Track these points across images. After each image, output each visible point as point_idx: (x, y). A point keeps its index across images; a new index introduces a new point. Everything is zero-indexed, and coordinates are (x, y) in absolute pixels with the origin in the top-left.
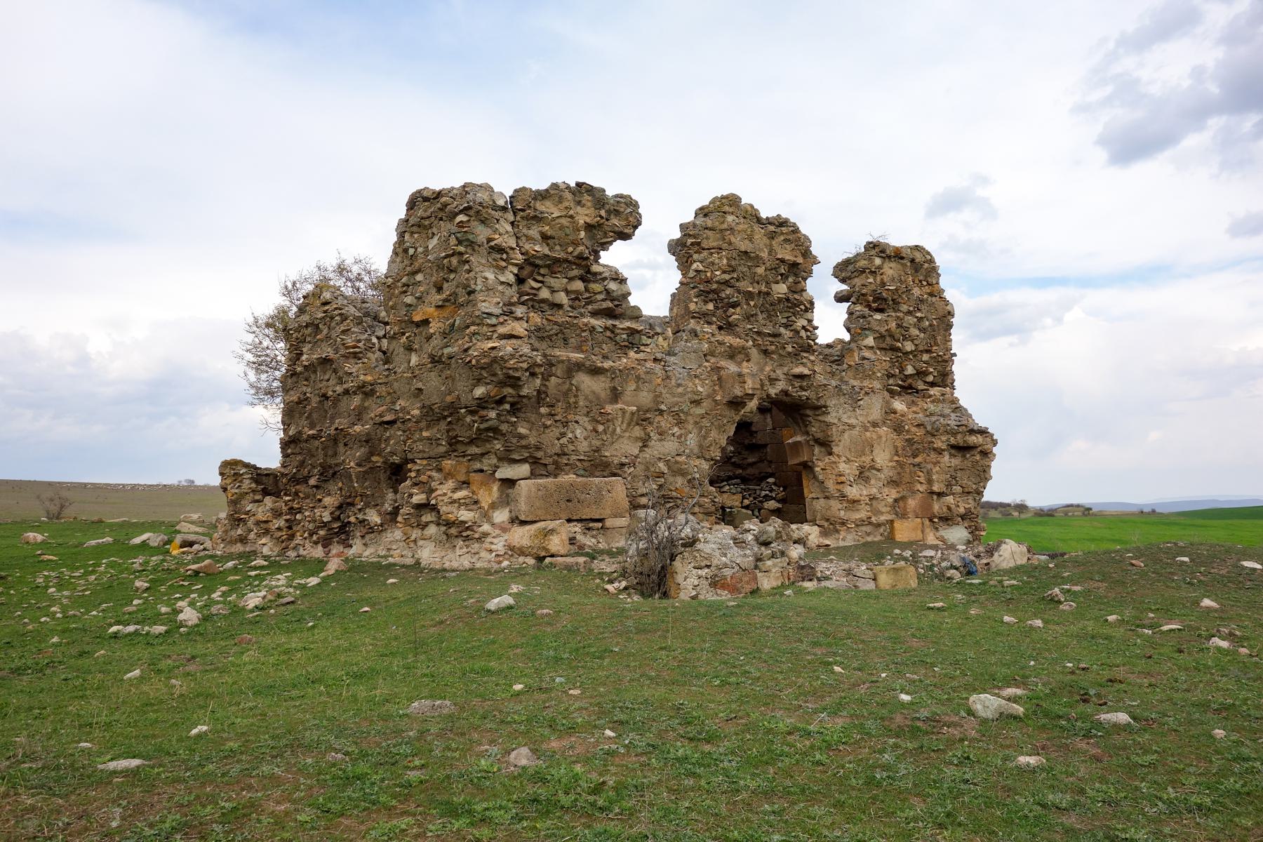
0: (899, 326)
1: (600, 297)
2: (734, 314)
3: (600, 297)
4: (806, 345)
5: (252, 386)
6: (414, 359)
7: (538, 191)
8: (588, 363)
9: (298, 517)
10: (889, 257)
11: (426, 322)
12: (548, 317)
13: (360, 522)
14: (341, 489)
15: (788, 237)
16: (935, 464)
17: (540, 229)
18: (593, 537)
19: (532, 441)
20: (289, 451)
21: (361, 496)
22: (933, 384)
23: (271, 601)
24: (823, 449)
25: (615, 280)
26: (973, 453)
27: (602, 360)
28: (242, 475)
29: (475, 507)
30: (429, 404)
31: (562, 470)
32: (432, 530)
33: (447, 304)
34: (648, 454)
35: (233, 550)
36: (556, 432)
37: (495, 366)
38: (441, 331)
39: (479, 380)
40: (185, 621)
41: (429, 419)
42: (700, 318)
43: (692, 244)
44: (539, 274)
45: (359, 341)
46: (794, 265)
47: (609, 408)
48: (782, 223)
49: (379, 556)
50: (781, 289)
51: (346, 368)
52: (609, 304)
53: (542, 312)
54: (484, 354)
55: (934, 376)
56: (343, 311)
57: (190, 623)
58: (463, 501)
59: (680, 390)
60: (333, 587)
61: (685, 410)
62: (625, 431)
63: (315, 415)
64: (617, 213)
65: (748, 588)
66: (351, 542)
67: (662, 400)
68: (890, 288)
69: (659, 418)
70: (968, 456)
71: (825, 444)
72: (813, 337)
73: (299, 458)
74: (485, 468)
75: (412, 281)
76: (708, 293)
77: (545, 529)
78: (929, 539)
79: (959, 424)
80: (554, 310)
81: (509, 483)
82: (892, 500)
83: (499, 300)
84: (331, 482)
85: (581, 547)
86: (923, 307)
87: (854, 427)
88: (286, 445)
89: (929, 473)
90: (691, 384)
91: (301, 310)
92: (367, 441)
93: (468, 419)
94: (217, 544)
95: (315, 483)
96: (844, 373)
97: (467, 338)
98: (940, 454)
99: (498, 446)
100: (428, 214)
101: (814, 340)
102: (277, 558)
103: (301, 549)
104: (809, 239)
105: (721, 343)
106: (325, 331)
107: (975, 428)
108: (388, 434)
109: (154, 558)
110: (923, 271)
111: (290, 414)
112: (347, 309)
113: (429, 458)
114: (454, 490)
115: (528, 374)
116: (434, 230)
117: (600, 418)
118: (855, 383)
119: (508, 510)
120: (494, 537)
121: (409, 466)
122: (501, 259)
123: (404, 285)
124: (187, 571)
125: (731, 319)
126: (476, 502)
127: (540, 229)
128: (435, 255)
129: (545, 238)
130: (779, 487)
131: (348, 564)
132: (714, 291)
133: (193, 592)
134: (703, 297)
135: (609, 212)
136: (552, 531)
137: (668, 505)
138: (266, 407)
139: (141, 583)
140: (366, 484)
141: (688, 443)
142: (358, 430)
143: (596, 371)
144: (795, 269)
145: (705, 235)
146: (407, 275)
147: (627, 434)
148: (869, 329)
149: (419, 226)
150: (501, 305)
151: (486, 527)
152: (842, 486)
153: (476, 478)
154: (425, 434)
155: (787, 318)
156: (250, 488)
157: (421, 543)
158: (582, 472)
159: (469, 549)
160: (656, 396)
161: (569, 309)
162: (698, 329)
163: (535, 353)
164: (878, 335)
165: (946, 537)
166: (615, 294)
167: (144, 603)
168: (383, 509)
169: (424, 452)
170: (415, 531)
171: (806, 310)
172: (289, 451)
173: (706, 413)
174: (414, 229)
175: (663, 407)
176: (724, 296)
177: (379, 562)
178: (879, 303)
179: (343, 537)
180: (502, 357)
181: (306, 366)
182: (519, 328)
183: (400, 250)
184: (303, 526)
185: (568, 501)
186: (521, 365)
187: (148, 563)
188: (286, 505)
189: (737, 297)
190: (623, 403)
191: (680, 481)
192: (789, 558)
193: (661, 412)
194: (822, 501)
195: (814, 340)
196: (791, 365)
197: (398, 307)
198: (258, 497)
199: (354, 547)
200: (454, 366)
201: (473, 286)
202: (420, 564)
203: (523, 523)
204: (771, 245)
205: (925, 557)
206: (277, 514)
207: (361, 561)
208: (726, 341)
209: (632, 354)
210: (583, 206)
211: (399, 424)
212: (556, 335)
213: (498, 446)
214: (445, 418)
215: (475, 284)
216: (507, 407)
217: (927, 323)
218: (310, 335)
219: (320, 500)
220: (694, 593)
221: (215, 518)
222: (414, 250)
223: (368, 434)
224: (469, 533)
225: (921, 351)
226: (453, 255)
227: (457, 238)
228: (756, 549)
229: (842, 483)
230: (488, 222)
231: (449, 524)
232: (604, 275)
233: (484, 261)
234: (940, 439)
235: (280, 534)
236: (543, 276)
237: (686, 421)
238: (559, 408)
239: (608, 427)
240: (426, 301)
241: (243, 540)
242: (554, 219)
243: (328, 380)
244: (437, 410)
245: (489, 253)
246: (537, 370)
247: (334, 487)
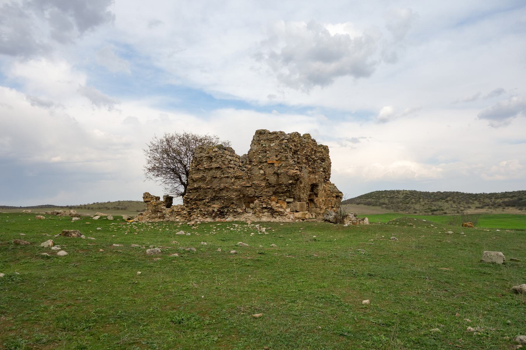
16: (333, 200)
81: (288, 203)
89: (331, 202)
99: (288, 194)
151: (286, 213)
154: (265, 190)
157: (263, 217)
169: (266, 194)
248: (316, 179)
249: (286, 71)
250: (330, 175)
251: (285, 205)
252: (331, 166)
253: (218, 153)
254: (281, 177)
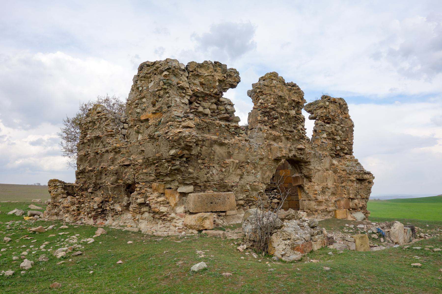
0: (335, 130)
1: (223, 112)
2: (276, 122)
3: (223, 112)
4: (302, 137)
5: (65, 148)
6: (140, 137)
7: (199, 64)
8: (219, 141)
9: (82, 205)
10: (331, 102)
11: (147, 120)
12: (202, 119)
13: (111, 210)
14: (103, 194)
16: (350, 186)
17: (200, 80)
18: (221, 219)
19: (195, 175)
20: (79, 177)
21: (112, 198)
22: (346, 154)
23: (69, 253)
24: (307, 180)
25: (230, 105)
26: (365, 182)
27: (224, 139)
28: (58, 186)
29: (168, 205)
30: (147, 157)
31: (207, 188)
32: (146, 215)
33: (157, 112)
34: (242, 182)
35: (52, 218)
36: (205, 171)
37: (181, 140)
38: (155, 124)
39: (172, 147)
40: (24, 267)
41: (146, 164)
42: (262, 123)
43: (259, 92)
44: (198, 100)
45: (113, 129)
46: (298, 103)
47: (227, 161)
49: (120, 226)
50: (293, 112)
51: (107, 141)
52: (227, 115)
53: (199, 117)
54: (175, 135)
55: (347, 151)
56: (106, 116)
57: (26, 268)
58: (162, 202)
59: (255, 153)
60: (101, 244)
61: (257, 162)
62: (234, 171)
63: (92, 162)
64: (230, 76)
65: (309, 250)
66: (107, 218)
67: (248, 158)
68: (332, 114)
69: (247, 166)
70: (363, 183)
71: (309, 178)
72: (304, 133)
73: (84, 180)
74: (172, 187)
75: (140, 102)
76: (266, 112)
77: (202, 217)
78: (349, 217)
79: (361, 170)
80: (204, 117)
81: (184, 194)
82: (334, 201)
83: (182, 111)
84: (98, 191)
85: (218, 225)
86: (343, 122)
87: (320, 170)
88: (78, 174)
89: (348, 190)
90: (260, 151)
91: (88, 116)
92: (116, 173)
93: (166, 165)
94: (45, 215)
95: (91, 191)
96: (316, 148)
97: (167, 127)
98: (353, 182)
99: (179, 177)
100: (149, 71)
101: (305, 134)
102: (72, 224)
103: (83, 220)
104: (303, 93)
105: (271, 134)
106: (98, 125)
107: (366, 172)
108: (126, 170)
109: (17, 222)
110: (343, 108)
111: (81, 160)
112: (108, 115)
113: (146, 182)
114: (158, 197)
115: (195, 144)
116: (152, 79)
117: (223, 165)
118: (320, 152)
119: (183, 207)
120: (177, 220)
121: (136, 185)
122: (183, 92)
123: (136, 104)
124: (30, 231)
125: (274, 124)
126: (168, 203)
127: (200, 80)
128: (152, 90)
129: (202, 84)
130: (278, 193)
131: (106, 230)
132: (268, 112)
133: (31, 244)
134: (263, 114)
135: (227, 75)
136: (206, 218)
137: (250, 204)
138: (70, 157)
139: (7, 238)
140: (115, 193)
141: (258, 177)
142: (112, 168)
143: (222, 144)
144: (298, 105)
145: (264, 88)
146: (138, 99)
147: (234, 173)
148: (324, 131)
149: (145, 77)
150: (183, 113)
151: (173, 215)
152: (316, 195)
153: (168, 192)
154: (144, 171)
155: (295, 124)
156: (61, 192)
157: (141, 221)
158: (215, 189)
159: (165, 225)
160: (246, 156)
161: (210, 116)
162: (262, 127)
163: (198, 135)
164: (328, 133)
165: (355, 217)
166: (229, 111)
167: (7, 251)
168: (122, 204)
169: (144, 179)
170: (138, 215)
171: (302, 122)
172: (79, 177)
173: (265, 164)
174: (143, 79)
175: (249, 161)
176: (272, 114)
177: (120, 229)
178: (328, 120)
179: (103, 215)
180: (184, 136)
181: (89, 140)
182: (191, 124)
183: (135, 89)
184: (84, 210)
185: (211, 203)
186: (193, 140)
187: (14, 225)
188: (77, 200)
189: (277, 115)
190: (233, 159)
191: (255, 194)
192: (324, 234)
193: (248, 163)
194: (307, 201)
195: (305, 134)
196: (297, 144)
197: (133, 114)
198: (65, 196)
199: (108, 221)
200: (160, 140)
201: (170, 104)
202: (141, 231)
203: (191, 213)
204: (289, 94)
205: (360, 228)
206: (73, 204)
207: (112, 228)
208: (272, 133)
209: (236, 137)
210: (217, 72)
211: (132, 166)
212: (205, 127)
213: (179, 177)
214: (154, 164)
215: (171, 103)
216: (185, 159)
217: (345, 129)
218: (91, 126)
219: (93, 199)
220: (283, 253)
221: (46, 201)
222: (142, 88)
223: (116, 170)
224: (165, 217)
225: (342, 140)
226: (161, 90)
227: (163, 82)
228: (309, 230)
229: (316, 194)
230: (177, 76)
231: (155, 213)
232: (225, 103)
233: (175, 93)
234: (353, 176)
235: (74, 213)
236: (200, 101)
237: (257, 167)
238: (206, 161)
239: (227, 169)
240: (147, 111)
241: (57, 214)
242: (206, 76)
243: (99, 146)
244: (151, 160)
245: (178, 89)
246: (199, 143)
247: (99, 193)
248: (281, 150)
249: (406, 65)
250: (352, 145)
251: (174, 199)
252: (353, 131)
253: (102, 115)
254: (159, 144)
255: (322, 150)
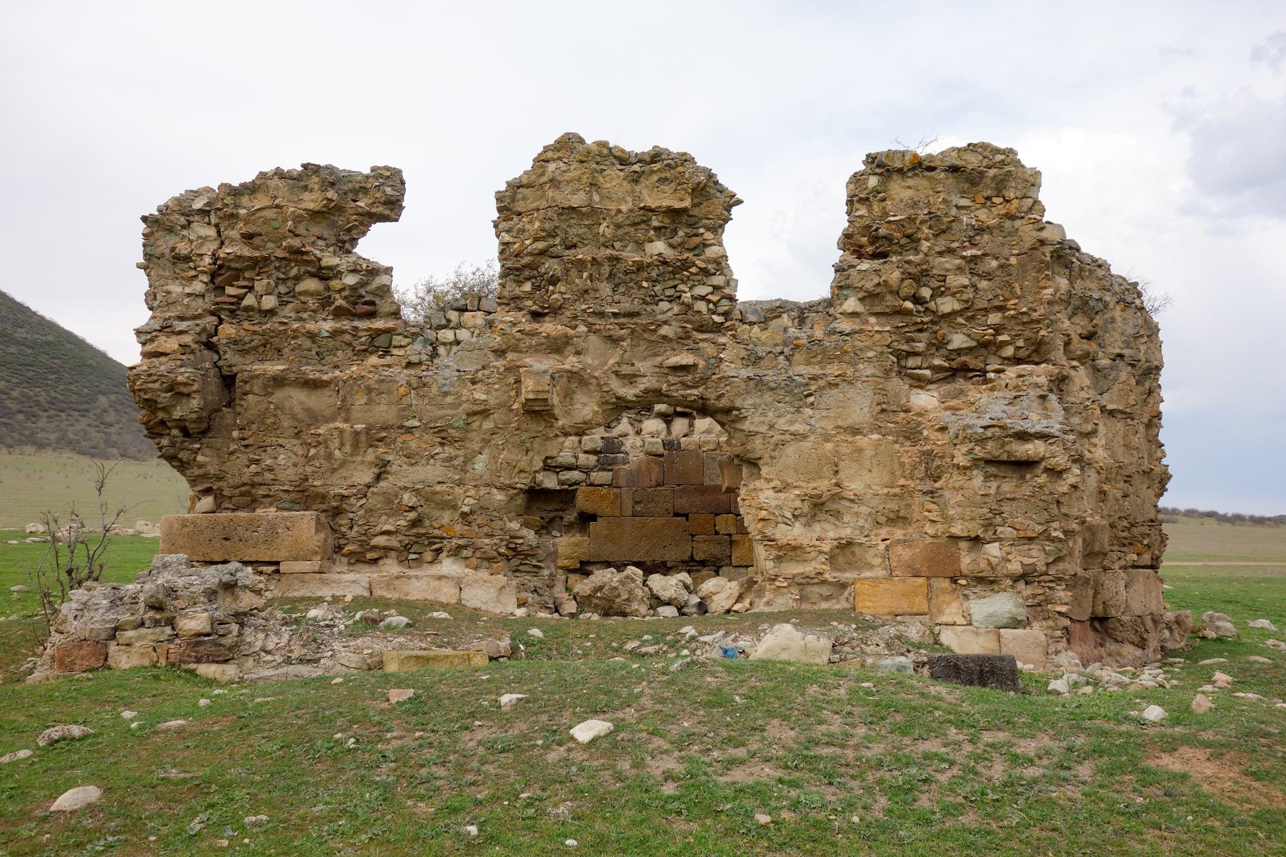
15: (663, 175)
19: (212, 470)
48: (656, 156)
59: (449, 399)
70: (1028, 476)
129: (248, 237)
148: (848, 287)
155: (675, 287)
164: (861, 294)
185: (226, 539)
210: (311, 191)
255: (820, 362)
